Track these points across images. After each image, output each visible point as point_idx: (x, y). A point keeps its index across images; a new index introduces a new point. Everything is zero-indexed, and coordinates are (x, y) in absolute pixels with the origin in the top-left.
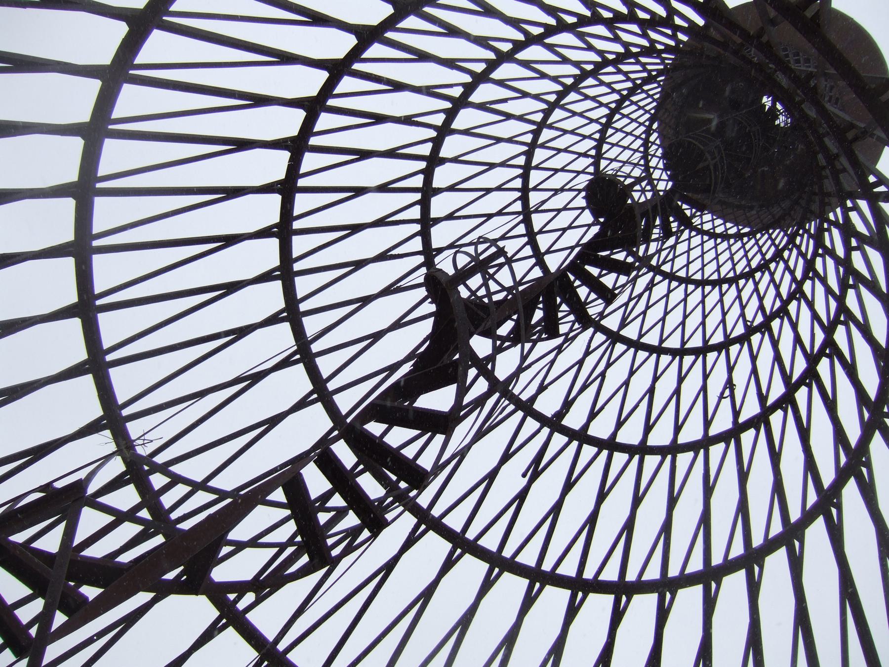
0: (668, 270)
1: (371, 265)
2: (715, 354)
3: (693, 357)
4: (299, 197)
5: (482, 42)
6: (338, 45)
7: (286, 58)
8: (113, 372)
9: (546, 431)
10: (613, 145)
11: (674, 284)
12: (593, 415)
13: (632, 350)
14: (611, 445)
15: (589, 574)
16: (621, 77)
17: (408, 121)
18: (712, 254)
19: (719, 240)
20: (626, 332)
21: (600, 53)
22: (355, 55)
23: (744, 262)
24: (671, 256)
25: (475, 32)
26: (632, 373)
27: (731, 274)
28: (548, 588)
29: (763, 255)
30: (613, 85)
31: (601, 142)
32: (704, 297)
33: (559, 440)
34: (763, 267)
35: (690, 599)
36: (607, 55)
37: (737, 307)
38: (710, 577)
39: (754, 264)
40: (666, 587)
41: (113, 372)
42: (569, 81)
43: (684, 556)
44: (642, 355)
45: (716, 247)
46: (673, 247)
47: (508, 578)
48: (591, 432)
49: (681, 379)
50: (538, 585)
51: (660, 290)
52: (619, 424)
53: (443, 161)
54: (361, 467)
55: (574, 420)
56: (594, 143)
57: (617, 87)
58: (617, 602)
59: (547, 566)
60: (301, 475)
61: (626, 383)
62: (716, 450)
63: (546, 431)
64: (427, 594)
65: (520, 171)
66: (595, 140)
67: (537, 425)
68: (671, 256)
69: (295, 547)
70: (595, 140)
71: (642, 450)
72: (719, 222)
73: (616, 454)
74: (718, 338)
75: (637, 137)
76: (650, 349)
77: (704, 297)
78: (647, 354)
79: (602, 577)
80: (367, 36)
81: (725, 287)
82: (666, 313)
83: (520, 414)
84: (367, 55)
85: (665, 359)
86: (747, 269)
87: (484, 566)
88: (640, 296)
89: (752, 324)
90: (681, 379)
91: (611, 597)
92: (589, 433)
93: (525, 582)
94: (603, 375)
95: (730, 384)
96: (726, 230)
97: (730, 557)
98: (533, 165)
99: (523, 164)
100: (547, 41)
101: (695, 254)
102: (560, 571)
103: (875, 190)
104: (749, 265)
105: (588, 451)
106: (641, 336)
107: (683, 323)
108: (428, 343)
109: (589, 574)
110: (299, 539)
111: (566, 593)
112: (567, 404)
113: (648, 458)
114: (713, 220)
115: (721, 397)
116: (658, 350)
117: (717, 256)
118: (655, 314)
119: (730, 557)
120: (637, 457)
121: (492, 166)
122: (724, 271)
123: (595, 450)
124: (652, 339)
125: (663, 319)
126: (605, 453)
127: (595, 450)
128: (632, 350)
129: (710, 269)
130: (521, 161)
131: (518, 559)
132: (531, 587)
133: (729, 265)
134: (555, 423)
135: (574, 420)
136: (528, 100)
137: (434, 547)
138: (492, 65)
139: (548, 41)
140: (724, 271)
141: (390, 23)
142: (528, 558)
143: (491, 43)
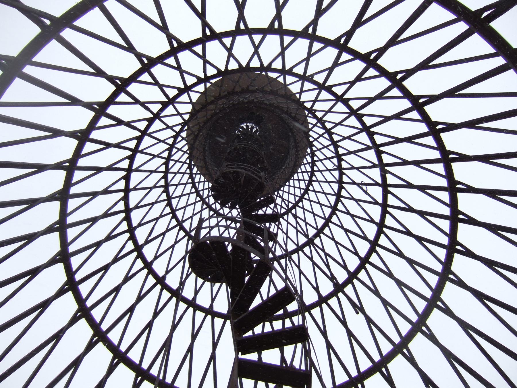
1: (41, 238)
4: (110, 335)
10: (176, 173)
13: (322, 235)
14: (364, 261)
24: (287, 202)
28: (428, 322)
44: (326, 231)
46: (283, 200)
50: (424, 328)
51: (299, 212)
52: (317, 289)
53: (164, 277)
55: (341, 276)
63: (340, 295)
68: (287, 202)
71: (374, 244)
73: (371, 260)
75: (184, 163)
78: (327, 228)
79: (434, 286)
83: (324, 305)
85: (334, 219)
88: (297, 223)
89: (336, 166)
93: (419, 335)
94: (326, 254)
95: (360, 185)
97: (444, 174)
105: (362, 275)
112: (332, 278)
113: (380, 242)
114: (289, 186)
115: (366, 192)
116: (328, 221)
118: (310, 218)
119: (444, 174)
124: (321, 222)
127: (363, 271)
131: (403, 334)
134: (339, 288)
135: (341, 276)
142: (405, 328)
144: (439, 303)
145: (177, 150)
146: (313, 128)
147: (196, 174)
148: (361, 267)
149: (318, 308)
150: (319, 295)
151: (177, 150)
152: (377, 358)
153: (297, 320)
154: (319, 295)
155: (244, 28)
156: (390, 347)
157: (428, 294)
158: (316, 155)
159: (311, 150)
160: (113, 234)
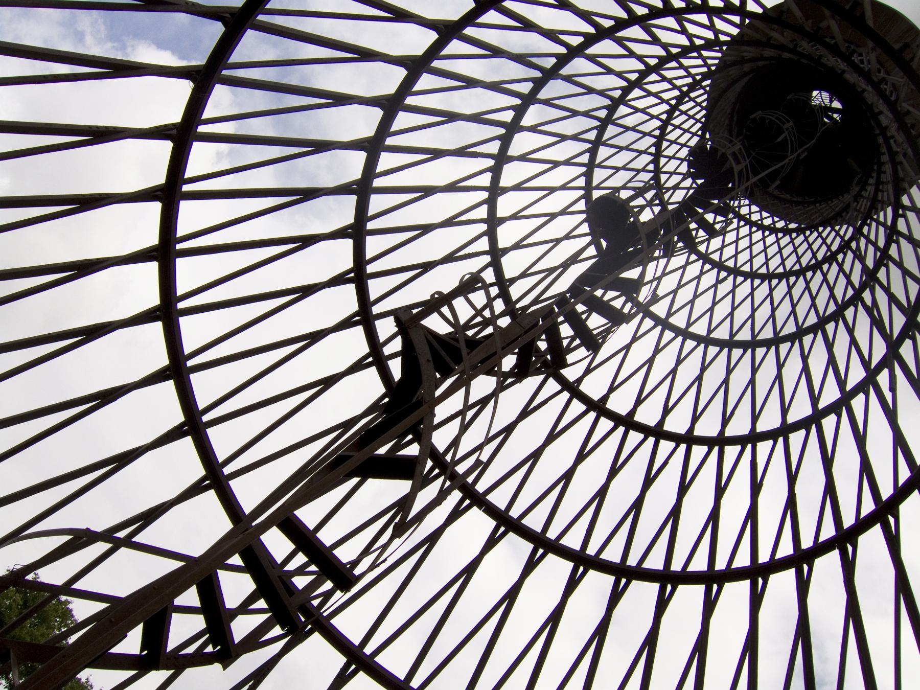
2: (789, 344)
3: (764, 349)
5: (551, 35)
6: (417, 40)
7: (365, 55)
11: (740, 279)
14: (657, 432)
15: (677, 566)
16: (682, 73)
17: (476, 118)
18: (775, 248)
19: (767, 233)
20: (675, 320)
21: (665, 46)
22: (434, 51)
23: (809, 254)
25: (546, 25)
26: (679, 362)
27: (797, 267)
28: (550, 557)
29: (829, 247)
30: (674, 81)
31: (660, 139)
32: (771, 290)
34: (830, 258)
35: (782, 584)
36: (671, 49)
37: (806, 298)
38: (802, 560)
39: (820, 256)
40: (758, 573)
42: (633, 77)
43: (770, 541)
44: (713, 350)
45: (750, 234)
47: (593, 575)
48: (697, 432)
49: (754, 370)
52: (666, 411)
56: (654, 140)
57: (678, 83)
59: (632, 561)
61: (674, 372)
62: (797, 438)
64: (511, 595)
65: (584, 169)
66: (654, 137)
70: (654, 137)
72: (754, 208)
73: (632, 433)
74: (790, 328)
76: (721, 344)
77: (771, 290)
79: (690, 568)
80: (447, 31)
81: (792, 279)
82: (714, 303)
83: (592, 415)
84: (446, 51)
85: (737, 353)
86: (813, 261)
87: (569, 566)
90: (754, 370)
92: (180, 319)
93: (611, 579)
96: (762, 219)
98: (597, 162)
99: (586, 162)
101: (744, 243)
104: (849, 282)
107: (752, 316)
108: (595, 260)
113: (727, 449)
117: (766, 248)
119: (820, 540)
120: (716, 449)
121: (556, 164)
122: (789, 264)
123: (641, 436)
125: (711, 309)
126: (683, 447)
128: (680, 339)
129: (774, 263)
130: (585, 158)
131: (603, 556)
133: (793, 258)
136: (594, 96)
137: (515, 549)
138: (563, 60)
140: (789, 264)
141: (470, 19)
142: (613, 554)
143: (561, 37)
144: (715, 587)
147: (704, 88)
148: (618, 420)
149: (583, 408)
150: (605, 398)
152: (552, 534)
153: (386, 328)
154: (605, 398)
156: (577, 546)
157: (676, 566)
158: (830, 265)
159: (793, 230)
160: (561, 37)
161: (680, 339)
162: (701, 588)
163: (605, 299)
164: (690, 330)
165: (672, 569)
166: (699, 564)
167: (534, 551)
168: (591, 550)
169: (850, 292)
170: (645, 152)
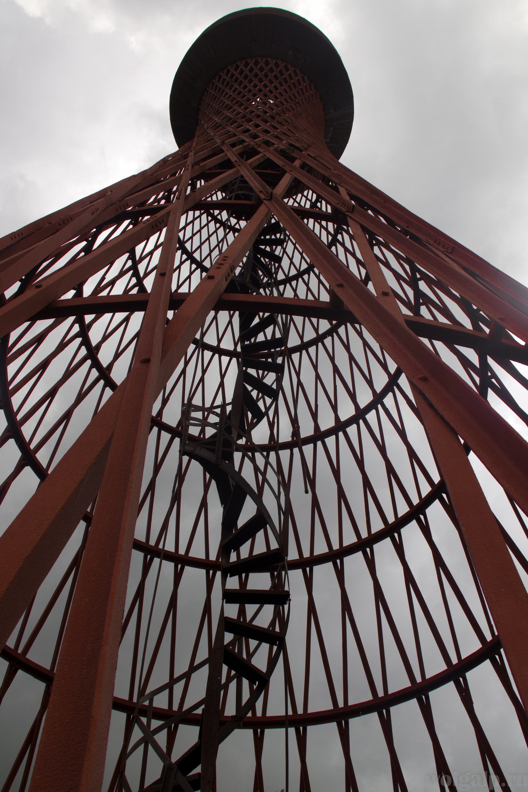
0: (284, 277)
8: (30, 656)
9: (296, 450)
12: (315, 416)
31: (190, 256)
33: (308, 449)
41: (30, 656)
44: (312, 350)
50: (368, 550)
54: (211, 572)
55: (307, 429)
58: (419, 522)
59: (364, 535)
60: (226, 617)
63: (296, 450)
66: (186, 260)
67: (288, 451)
69: (235, 680)
70: (186, 260)
79: (400, 515)
85: (328, 341)
91: (414, 522)
94: (300, 383)
100: (142, 275)
102: (374, 531)
103: (395, 387)
105: (330, 441)
106: (301, 337)
109: (391, 519)
110: (233, 672)
111: (388, 541)
112: (294, 421)
124: (293, 272)
126: (341, 434)
127: (334, 437)
128: (304, 352)
131: (345, 544)
132: (365, 554)
135: (307, 429)
139: (142, 275)
142: (350, 539)
144: (396, 535)
145: (238, 225)
146: (297, 202)
151: (238, 225)
152: (306, 554)
155: (199, 338)
156: (326, 550)
161: (304, 352)
162: (388, 540)
163: (269, 338)
164: (305, 340)
165: (390, 523)
166: (403, 509)
167: (304, 572)
168: (336, 546)
169: (330, 238)
170: (217, 229)
